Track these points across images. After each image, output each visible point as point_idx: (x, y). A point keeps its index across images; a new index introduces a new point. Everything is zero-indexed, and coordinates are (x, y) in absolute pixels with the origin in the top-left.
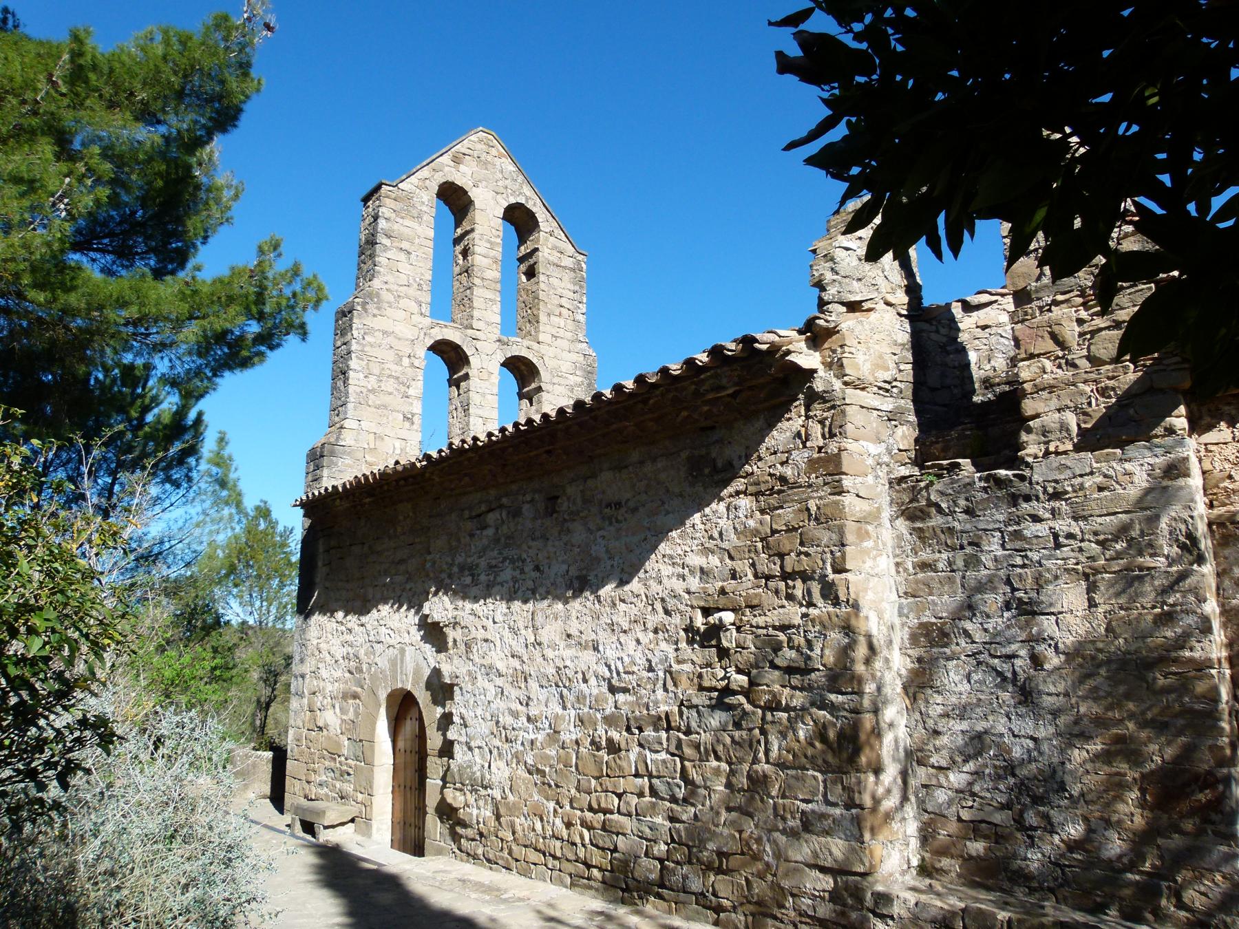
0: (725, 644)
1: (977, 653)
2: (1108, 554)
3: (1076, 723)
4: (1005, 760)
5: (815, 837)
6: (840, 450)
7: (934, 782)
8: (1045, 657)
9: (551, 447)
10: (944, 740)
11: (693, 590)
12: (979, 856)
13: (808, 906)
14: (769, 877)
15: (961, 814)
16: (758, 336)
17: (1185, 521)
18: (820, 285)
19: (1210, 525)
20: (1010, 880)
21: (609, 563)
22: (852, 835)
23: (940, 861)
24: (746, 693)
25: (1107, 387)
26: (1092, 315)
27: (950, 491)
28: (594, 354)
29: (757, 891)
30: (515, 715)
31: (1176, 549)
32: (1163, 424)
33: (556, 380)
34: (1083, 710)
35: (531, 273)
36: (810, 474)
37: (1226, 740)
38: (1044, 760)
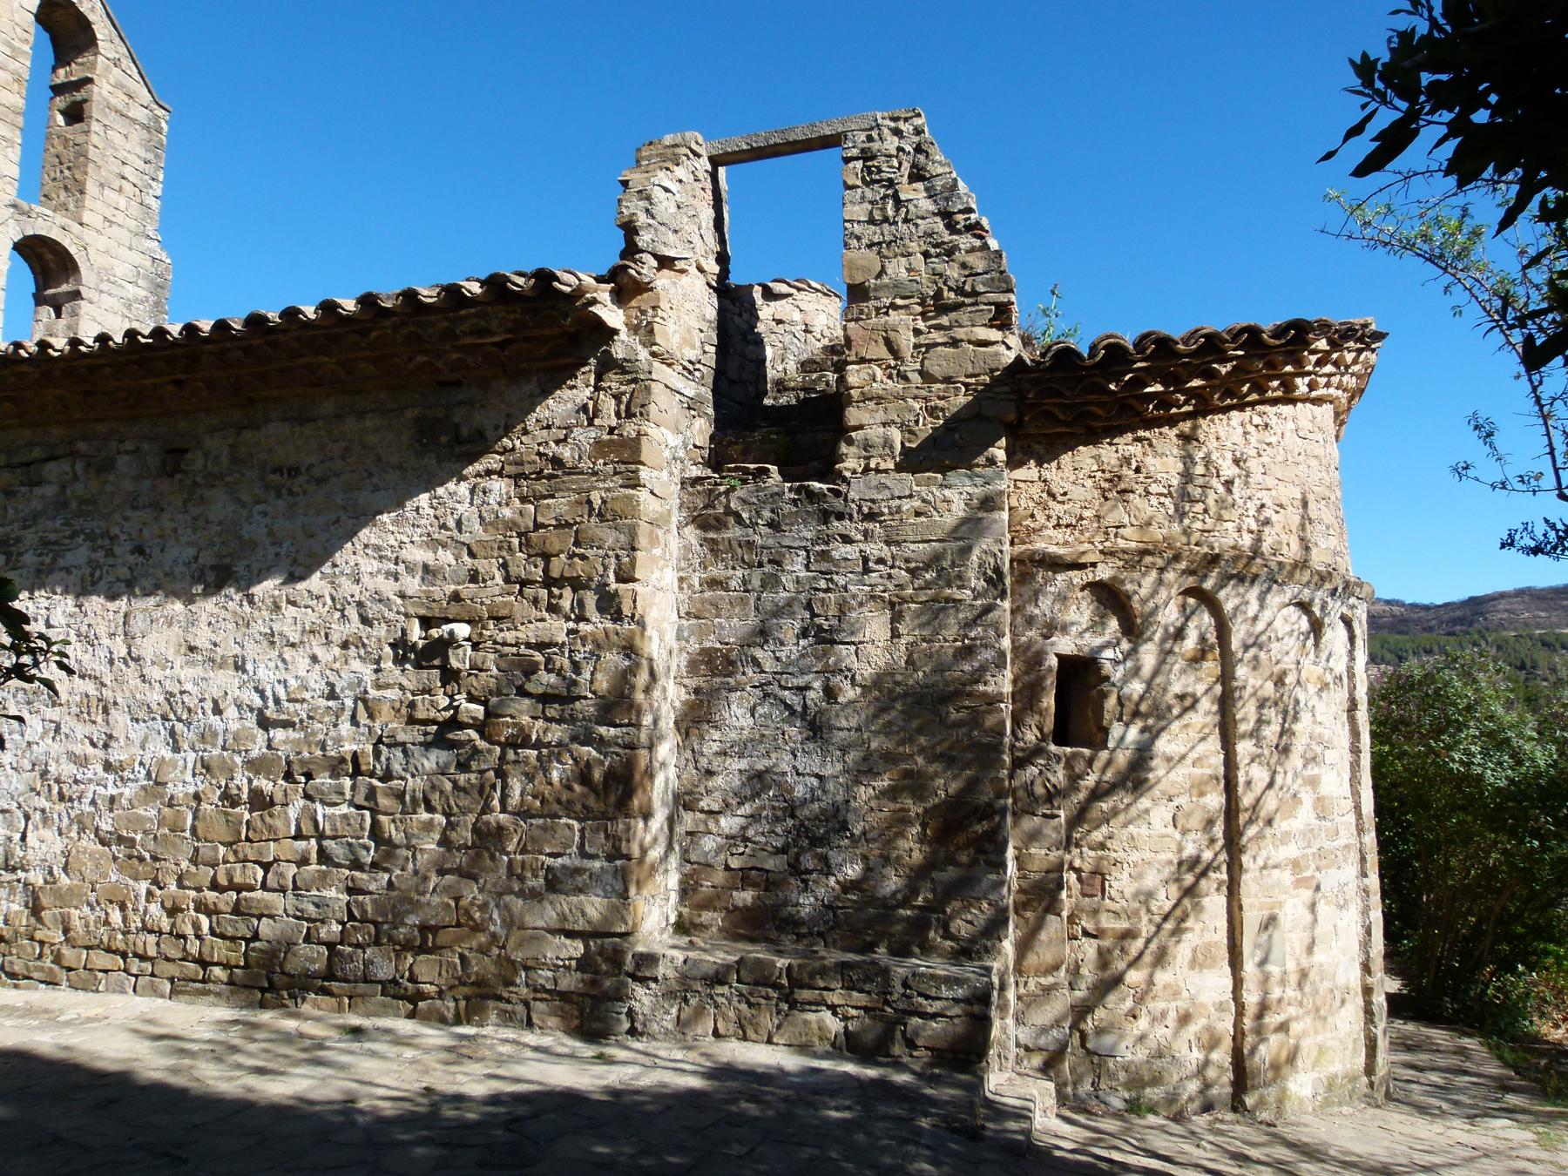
0: (455, 663)
1: (765, 684)
2: (917, 583)
3: (865, 759)
4: (785, 801)
5: (563, 897)
6: (639, 434)
7: (702, 829)
8: (840, 689)
9: (183, 377)
10: (719, 781)
11: (409, 592)
12: (745, 907)
13: (547, 979)
14: (495, 951)
15: (730, 862)
16: (559, 274)
18: (630, 229)
19: (1012, 561)
20: (778, 928)
21: (272, 550)
22: (614, 890)
23: (700, 916)
24: (481, 727)
25: (936, 407)
26: (930, 327)
27: (755, 500)
28: (168, 261)
29: (476, 969)
30: (82, 761)
33: (105, 286)
34: (874, 745)
35: (75, 114)
36: (596, 459)
38: (828, 799)
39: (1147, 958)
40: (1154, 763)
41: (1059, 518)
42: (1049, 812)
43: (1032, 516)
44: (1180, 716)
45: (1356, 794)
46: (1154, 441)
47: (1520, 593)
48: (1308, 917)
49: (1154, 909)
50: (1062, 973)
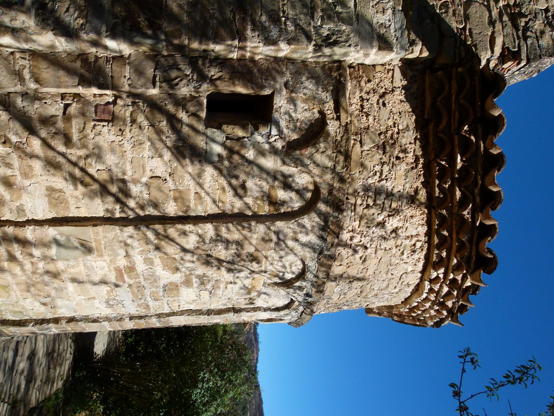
17: (347, 41)
25: (448, 8)
31: (326, 33)
32: (418, 39)
37: (186, 42)
39: (51, 154)
40: (198, 166)
41: (368, 100)
42: (157, 79)
43: (369, 81)
44: (230, 184)
45: (182, 313)
46: (415, 171)
47: (261, 400)
48: (97, 279)
49: (89, 160)
50: (33, 86)
